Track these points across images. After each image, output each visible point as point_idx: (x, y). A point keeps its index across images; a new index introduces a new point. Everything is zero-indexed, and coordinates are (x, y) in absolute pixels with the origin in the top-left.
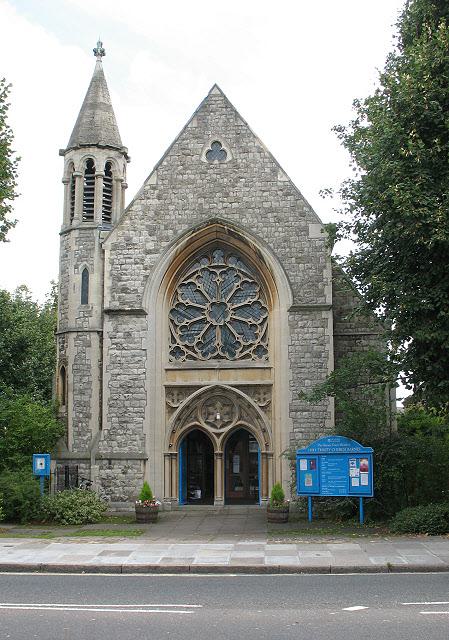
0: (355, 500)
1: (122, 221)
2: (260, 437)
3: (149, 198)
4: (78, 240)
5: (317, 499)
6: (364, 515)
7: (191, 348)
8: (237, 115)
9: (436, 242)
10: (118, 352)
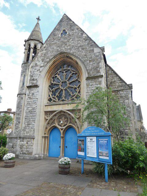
10: (29, 100)
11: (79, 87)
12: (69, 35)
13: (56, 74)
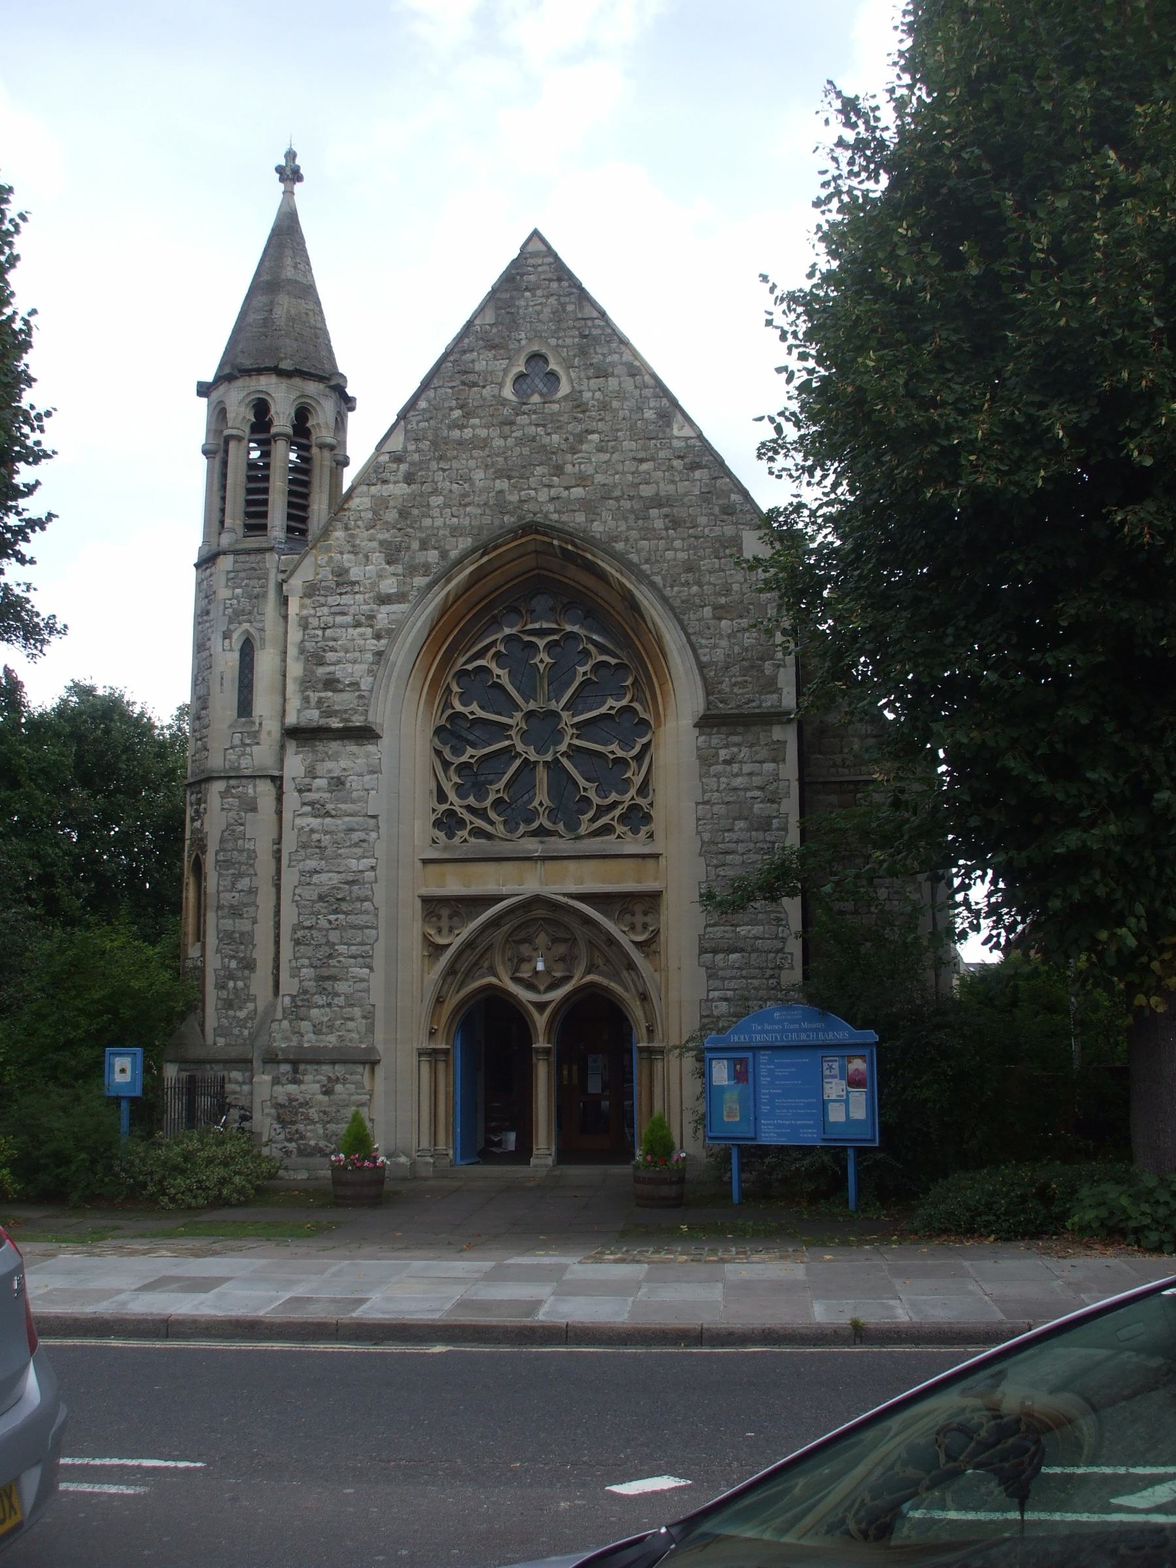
0: (837, 1154)
1: (326, 533)
2: (636, 1011)
3: (385, 482)
4: (233, 578)
5: (753, 1153)
6: (859, 1190)
7: (481, 813)
8: (583, 296)
9: (975, 492)
10: (315, 822)
11: (639, 758)
12: (578, 404)
13: (480, 654)
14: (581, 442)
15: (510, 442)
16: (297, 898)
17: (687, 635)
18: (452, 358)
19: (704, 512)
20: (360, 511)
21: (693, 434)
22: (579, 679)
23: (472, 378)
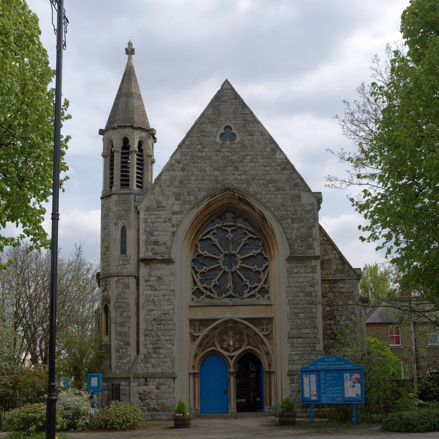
3: (174, 170)
8: (244, 105)
10: (152, 293)
11: (264, 271)
14: (244, 159)
15: (219, 158)
16: (145, 319)
17: (283, 228)
18: (197, 126)
19: (288, 185)
20: (165, 181)
21: (284, 158)
22: (243, 243)
23: (205, 133)
